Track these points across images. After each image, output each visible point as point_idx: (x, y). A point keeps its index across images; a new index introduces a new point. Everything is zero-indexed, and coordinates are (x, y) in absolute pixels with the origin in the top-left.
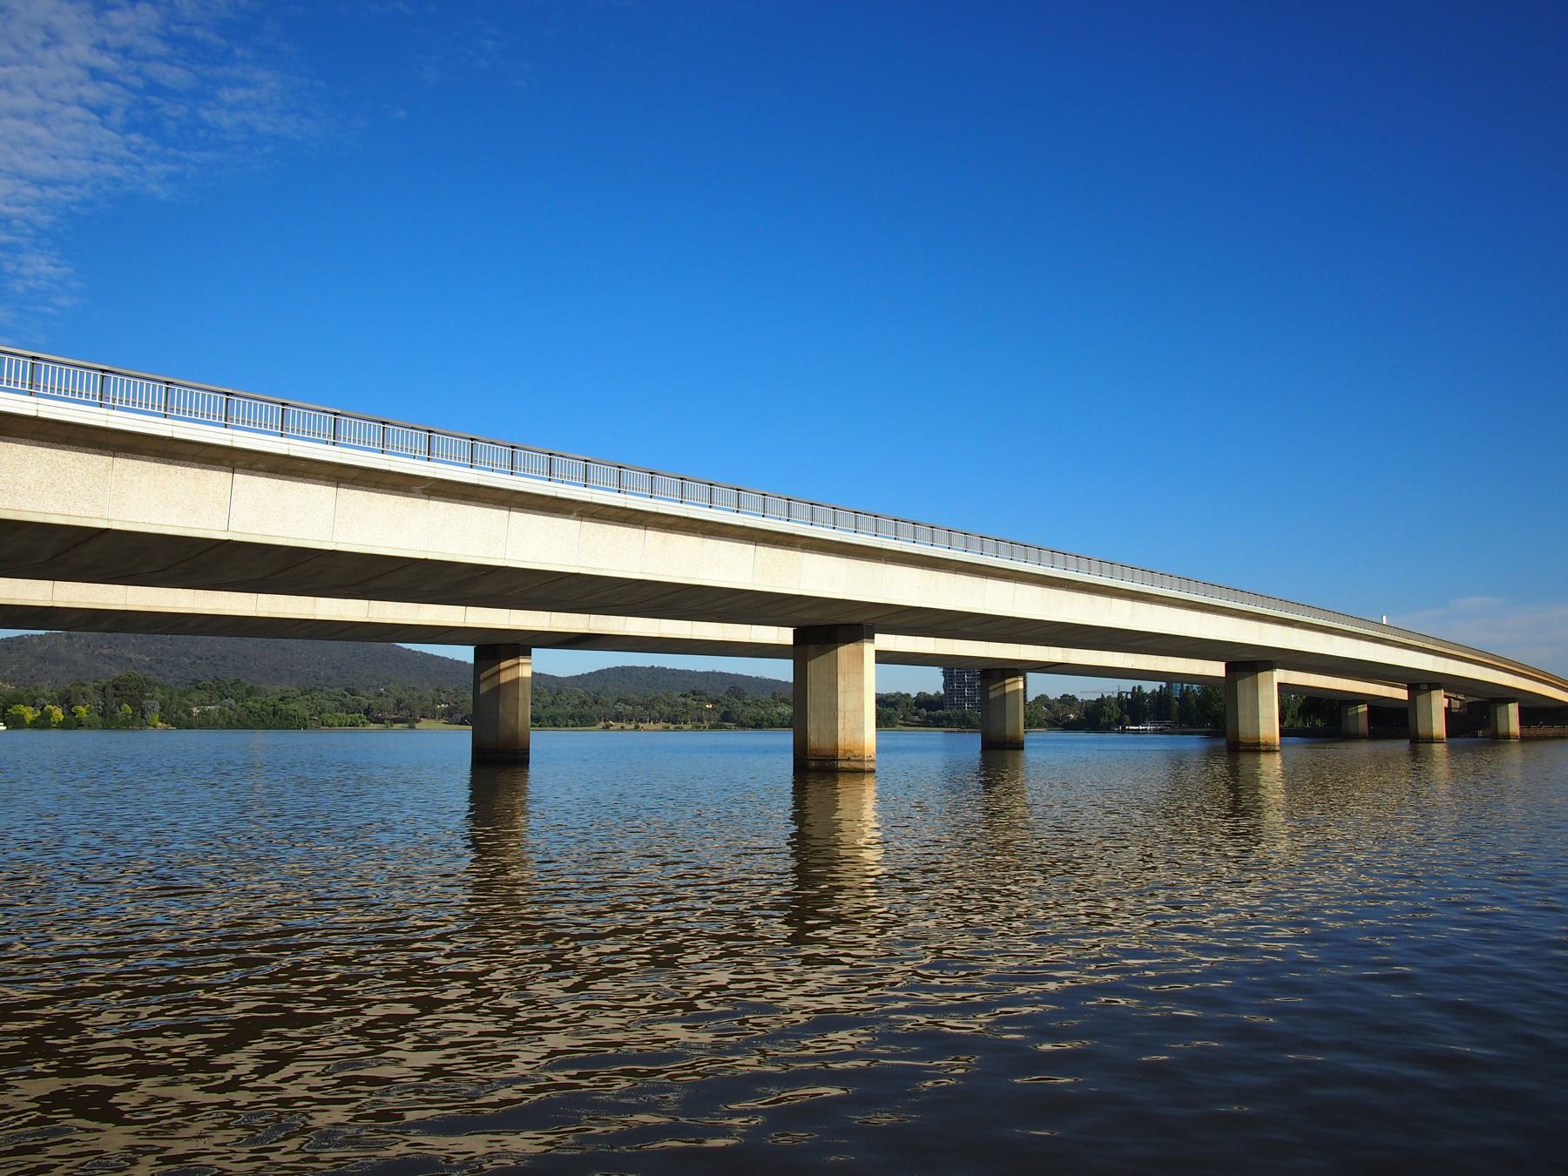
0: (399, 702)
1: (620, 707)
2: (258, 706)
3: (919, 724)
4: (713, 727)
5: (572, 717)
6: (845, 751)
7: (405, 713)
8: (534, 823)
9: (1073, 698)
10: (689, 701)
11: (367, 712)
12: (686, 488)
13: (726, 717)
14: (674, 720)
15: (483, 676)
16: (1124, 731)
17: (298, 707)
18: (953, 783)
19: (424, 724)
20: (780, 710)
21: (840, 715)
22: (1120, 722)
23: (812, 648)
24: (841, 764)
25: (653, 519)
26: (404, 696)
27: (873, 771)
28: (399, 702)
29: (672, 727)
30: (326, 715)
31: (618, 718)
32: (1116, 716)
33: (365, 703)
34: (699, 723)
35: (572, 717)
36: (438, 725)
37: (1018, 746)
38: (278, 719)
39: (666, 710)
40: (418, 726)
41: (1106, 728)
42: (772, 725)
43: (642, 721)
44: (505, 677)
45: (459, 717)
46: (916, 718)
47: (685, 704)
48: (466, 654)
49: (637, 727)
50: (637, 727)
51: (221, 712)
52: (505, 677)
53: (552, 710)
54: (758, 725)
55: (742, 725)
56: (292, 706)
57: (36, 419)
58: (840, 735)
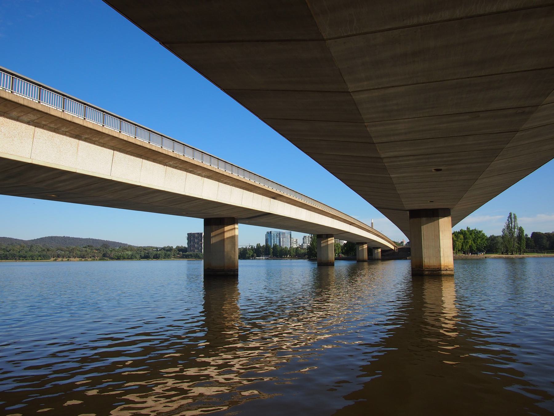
1: (59, 252)
3: (180, 258)
4: (100, 260)
5: (40, 256)
8: (202, 292)
10: (88, 249)
12: (115, 159)
13: (104, 255)
14: (83, 257)
15: (212, 234)
16: (255, 259)
18: (191, 278)
20: (127, 252)
21: (442, 250)
22: (253, 256)
23: (214, 227)
24: (443, 272)
27: (452, 275)
29: (83, 259)
31: (58, 256)
32: (251, 254)
34: (93, 258)
35: (40, 256)
37: (332, 264)
39: (79, 253)
41: (248, 258)
42: (124, 258)
43: (69, 257)
44: (227, 235)
46: (179, 255)
47: (86, 251)
49: (68, 260)
50: (68, 260)
52: (227, 235)
53: (31, 253)
54: (118, 258)
55: (112, 259)
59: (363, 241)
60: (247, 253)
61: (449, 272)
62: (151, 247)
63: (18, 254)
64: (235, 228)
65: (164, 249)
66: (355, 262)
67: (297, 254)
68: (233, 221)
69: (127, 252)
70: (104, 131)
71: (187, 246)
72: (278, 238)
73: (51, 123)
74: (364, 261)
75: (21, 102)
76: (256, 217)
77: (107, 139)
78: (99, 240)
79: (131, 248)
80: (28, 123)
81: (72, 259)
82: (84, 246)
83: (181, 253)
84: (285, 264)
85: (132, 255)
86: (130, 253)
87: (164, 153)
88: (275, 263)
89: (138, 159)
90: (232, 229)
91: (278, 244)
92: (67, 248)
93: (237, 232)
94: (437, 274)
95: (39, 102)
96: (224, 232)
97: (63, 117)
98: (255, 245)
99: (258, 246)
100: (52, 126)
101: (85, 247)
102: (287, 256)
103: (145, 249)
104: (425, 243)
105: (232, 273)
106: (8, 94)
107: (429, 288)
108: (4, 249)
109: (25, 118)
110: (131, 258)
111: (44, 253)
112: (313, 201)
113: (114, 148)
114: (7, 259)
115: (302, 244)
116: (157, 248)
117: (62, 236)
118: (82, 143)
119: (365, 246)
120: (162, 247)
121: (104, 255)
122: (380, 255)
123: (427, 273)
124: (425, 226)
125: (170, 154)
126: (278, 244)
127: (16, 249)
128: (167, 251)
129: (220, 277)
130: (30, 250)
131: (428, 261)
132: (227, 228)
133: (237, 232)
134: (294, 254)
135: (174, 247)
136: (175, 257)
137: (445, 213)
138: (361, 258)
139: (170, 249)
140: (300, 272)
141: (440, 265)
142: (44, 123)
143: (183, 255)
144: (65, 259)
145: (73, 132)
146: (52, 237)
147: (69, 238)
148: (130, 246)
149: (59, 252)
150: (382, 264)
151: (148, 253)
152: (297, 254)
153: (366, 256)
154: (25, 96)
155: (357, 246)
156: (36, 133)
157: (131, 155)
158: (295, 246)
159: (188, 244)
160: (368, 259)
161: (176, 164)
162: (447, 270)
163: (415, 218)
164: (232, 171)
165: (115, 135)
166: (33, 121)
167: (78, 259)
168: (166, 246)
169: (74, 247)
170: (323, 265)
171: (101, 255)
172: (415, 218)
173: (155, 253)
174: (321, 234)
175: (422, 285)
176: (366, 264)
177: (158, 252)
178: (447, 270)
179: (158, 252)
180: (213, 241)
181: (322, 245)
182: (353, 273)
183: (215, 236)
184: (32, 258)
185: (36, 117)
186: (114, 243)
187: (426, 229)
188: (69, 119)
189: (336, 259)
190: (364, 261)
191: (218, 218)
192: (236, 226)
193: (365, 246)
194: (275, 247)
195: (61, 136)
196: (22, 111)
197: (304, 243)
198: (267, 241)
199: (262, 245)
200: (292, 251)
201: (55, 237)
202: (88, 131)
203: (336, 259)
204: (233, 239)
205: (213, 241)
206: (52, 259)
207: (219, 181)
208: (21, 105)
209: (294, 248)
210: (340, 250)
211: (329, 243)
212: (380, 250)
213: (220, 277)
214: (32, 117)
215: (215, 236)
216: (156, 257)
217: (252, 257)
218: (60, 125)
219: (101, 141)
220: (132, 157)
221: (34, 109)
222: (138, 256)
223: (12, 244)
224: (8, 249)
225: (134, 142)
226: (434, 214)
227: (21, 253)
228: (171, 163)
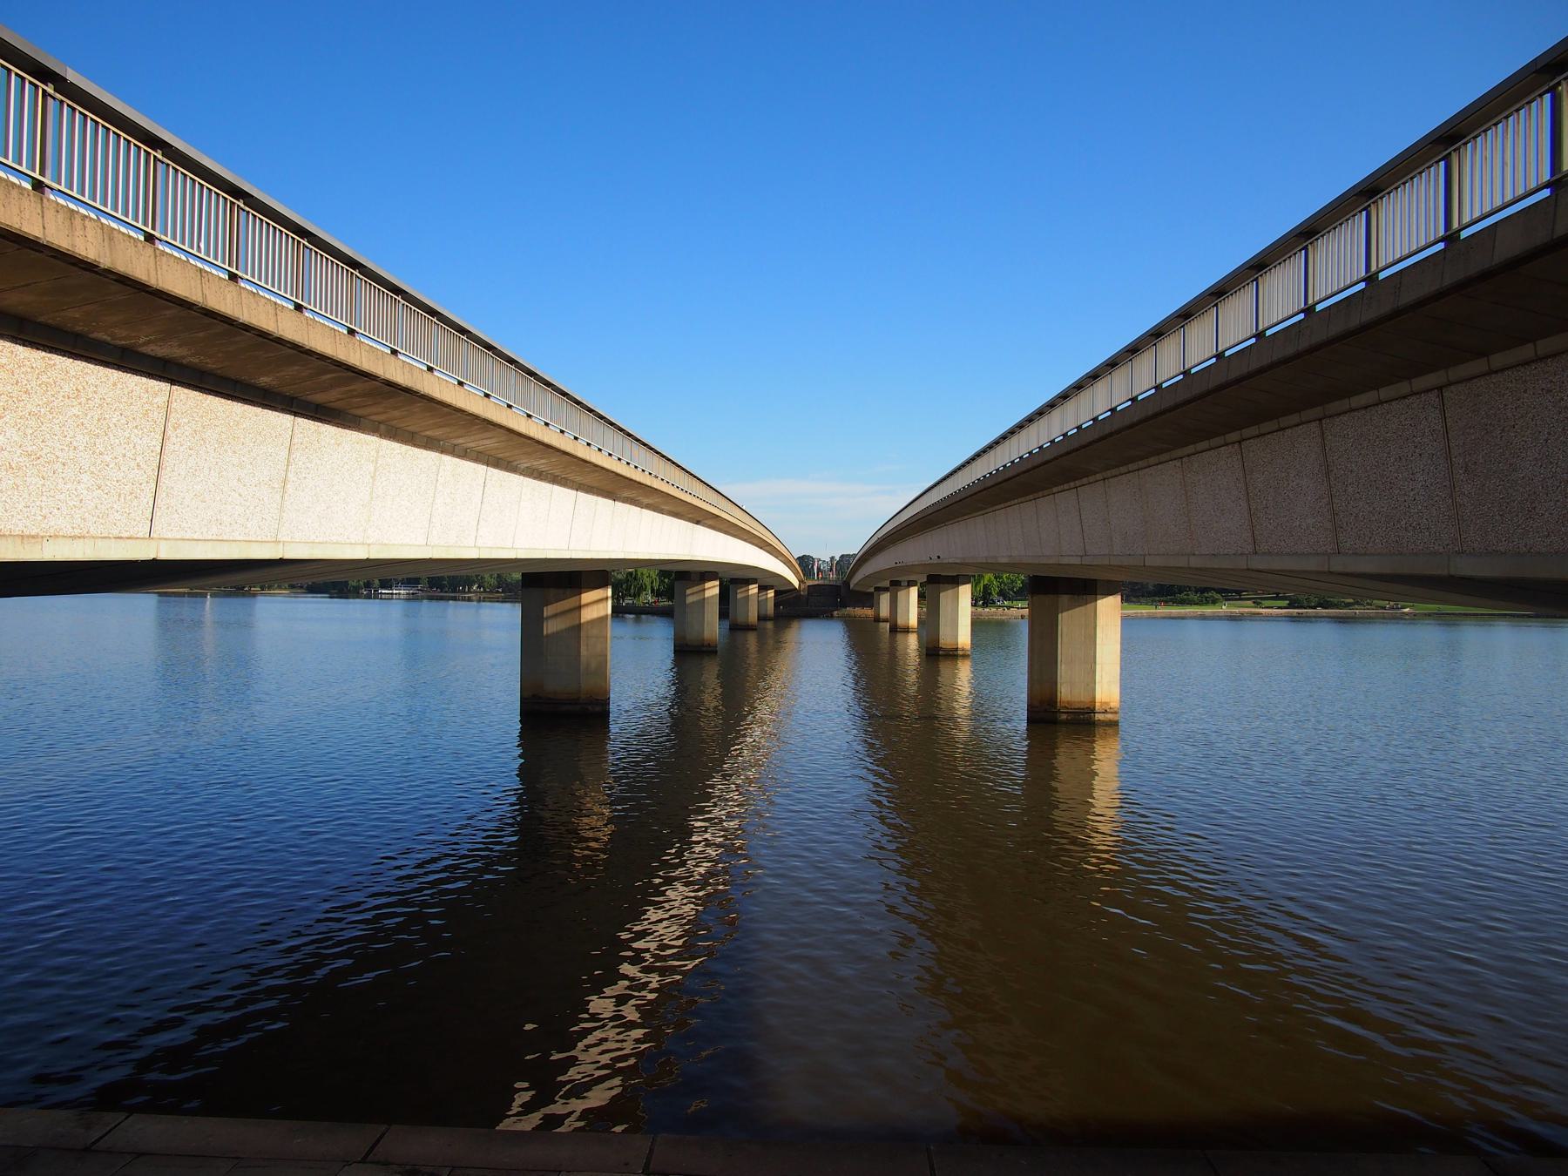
15: (548, 611)
23: (552, 592)
24: (1098, 717)
61: (1110, 716)
88: (429, 611)
95: (233, 277)
96: (580, 607)
105: (598, 709)
112: (565, 405)
123: (1064, 717)
134: (493, 582)
138: (740, 619)
154: (92, 214)
157: (598, 494)
175: (1053, 747)
180: (550, 627)
181: (690, 600)
183: (555, 616)
214: (488, 443)
215: (555, 616)
220: (594, 498)
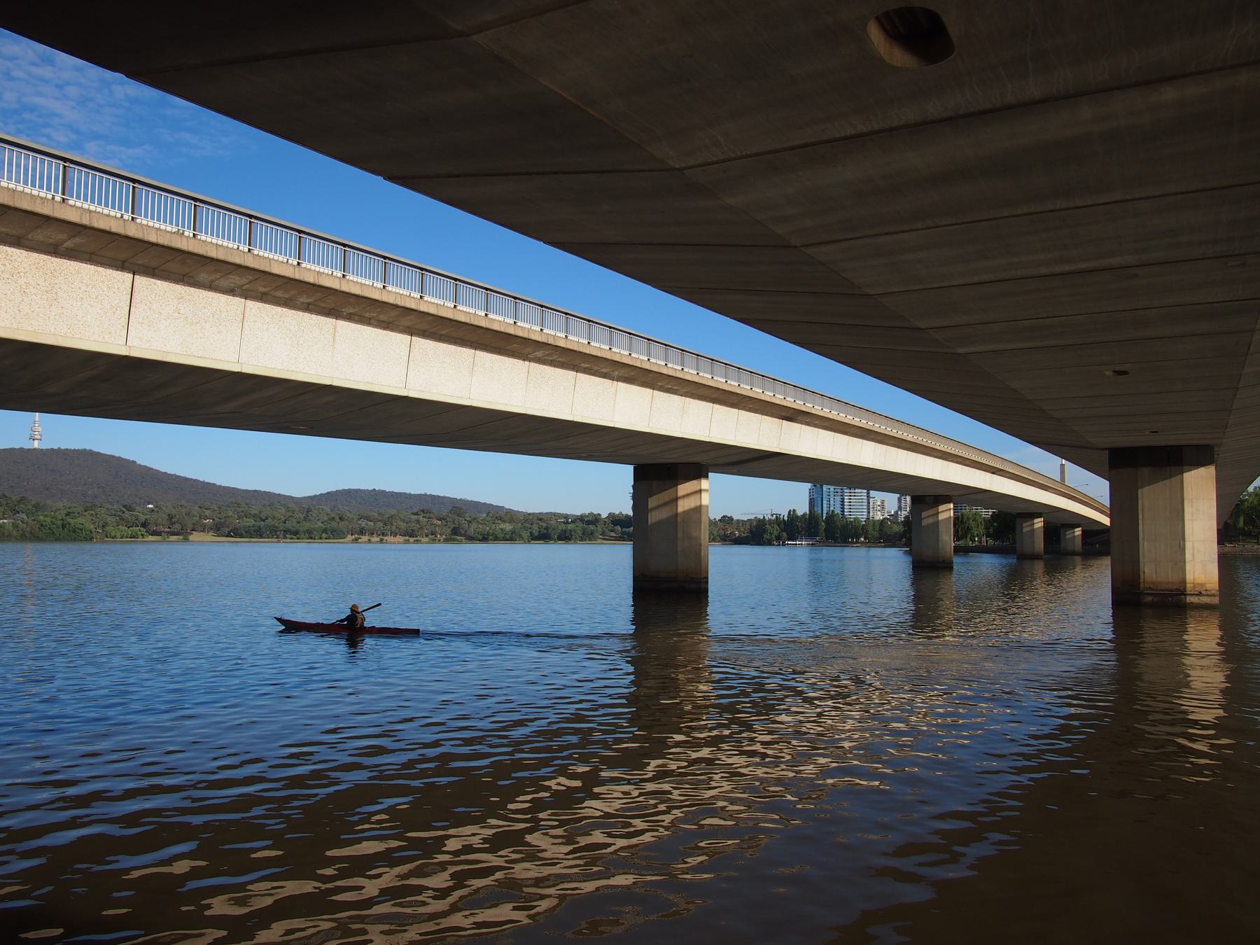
0: (171, 517)
1: (363, 523)
2: (49, 520)
3: (617, 539)
4: (446, 541)
5: (325, 531)
6: (1195, 585)
7: (177, 527)
9: (731, 519)
10: (421, 518)
11: (144, 525)
13: (455, 532)
14: (411, 534)
16: (784, 544)
17: (85, 521)
19: (195, 536)
20: (502, 526)
21: (1188, 545)
22: (778, 538)
24: (1190, 599)
25: (826, 424)
26: (173, 512)
28: (171, 517)
29: (412, 540)
30: (109, 529)
31: (362, 532)
32: (775, 533)
33: (142, 518)
34: (433, 536)
35: (325, 531)
36: (209, 537)
37: (947, 567)
38: (66, 532)
39: (403, 525)
40: (191, 538)
41: (769, 543)
42: (496, 539)
44: (683, 506)
45: (227, 530)
47: (418, 521)
48: (608, 488)
51: (15, 526)
52: (683, 506)
53: (306, 525)
54: (484, 538)
55: (471, 539)
56: (80, 520)
57: (406, 397)
58: (1188, 567)
59: (1032, 510)
60: (765, 531)
61: (1205, 600)
62: (555, 514)
63: (281, 526)
64: (700, 491)
65: (581, 519)
66: (1012, 560)
67: (881, 535)
68: (698, 472)
69: (502, 526)
70: (385, 299)
71: (631, 513)
72: (838, 498)
73: (275, 289)
74: (1035, 557)
75: (213, 254)
76: (748, 461)
77: (393, 313)
78: (444, 498)
79: (510, 516)
80: (231, 292)
81: (389, 538)
82: (415, 510)
83: (618, 528)
84: (855, 558)
85: (513, 532)
86: (508, 527)
87: (520, 334)
88: (830, 554)
89: (464, 350)
90: (695, 492)
91: (838, 511)
92: (380, 514)
93: (705, 499)
94: (1175, 603)
96: (677, 499)
97: (297, 277)
98: (784, 514)
99: (792, 514)
100: (279, 294)
101: (416, 514)
102: (858, 538)
103: (540, 517)
104: (1146, 527)
106: (185, 240)
107: (1154, 633)
108: (254, 516)
109: (223, 283)
110: (511, 538)
111: (334, 524)
113: (411, 331)
114: (261, 536)
115: (896, 513)
116: (566, 517)
117: (371, 488)
118: (342, 324)
119: (1039, 523)
120: (579, 514)
121: (455, 532)
122: (1079, 542)
123: (1149, 599)
124: (1146, 489)
125: (533, 337)
126: (838, 511)
127: (278, 515)
128: (589, 523)
129: (669, 591)
130: (305, 519)
131: (1152, 571)
132: (683, 489)
133: (705, 499)
134: (876, 534)
135: (604, 515)
136: (606, 538)
137: (1200, 456)
139: (593, 520)
140: (884, 576)
141: (1184, 582)
142: (262, 289)
143: (623, 533)
144: (375, 539)
145: (323, 305)
146: (349, 491)
147: (383, 493)
148: (509, 512)
149: (363, 523)
150: (1085, 567)
151: (547, 528)
152: (881, 535)
153: (1039, 544)
155: (1018, 521)
156: (248, 310)
158: (879, 517)
159: (634, 508)
160: (1046, 551)
161: (551, 355)
162: (1200, 594)
163: (1140, 465)
164: (682, 364)
165: (408, 305)
166: (240, 287)
167: (402, 539)
168: (587, 512)
169: (393, 512)
170: (928, 568)
171: (449, 531)
172: (1140, 465)
173: (563, 527)
174: (926, 495)
176: (1078, 559)
177: (570, 526)
178: (1200, 594)
179: (570, 526)
180: (653, 517)
181: (925, 523)
182: (1014, 582)
184: (310, 535)
185: (244, 280)
186: (476, 505)
187: (1150, 497)
188: (311, 280)
189: (957, 550)
190: (1035, 557)
191: (663, 465)
192: (705, 484)
193: (1039, 523)
194: (831, 517)
195: (300, 313)
196: (216, 271)
197: (900, 508)
198: (812, 502)
199: (800, 513)
200: (870, 529)
201: (357, 491)
202: (352, 300)
203: (957, 550)
204: (698, 510)
205: (653, 517)
206: (350, 538)
207: (652, 386)
208: (212, 259)
209: (874, 522)
210: (981, 530)
211: (942, 517)
212: (1078, 532)
213: (669, 591)
214: (236, 280)
216: (565, 537)
217: (779, 540)
218: (294, 292)
219: (382, 317)
221: (239, 266)
222: (526, 534)
223: (271, 505)
224: (263, 516)
225: (451, 317)
226: (1173, 460)
227: (289, 525)
228: (539, 354)
